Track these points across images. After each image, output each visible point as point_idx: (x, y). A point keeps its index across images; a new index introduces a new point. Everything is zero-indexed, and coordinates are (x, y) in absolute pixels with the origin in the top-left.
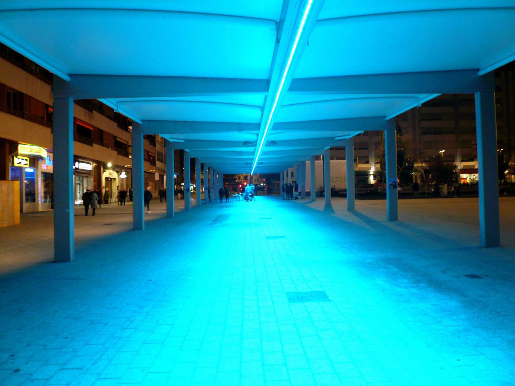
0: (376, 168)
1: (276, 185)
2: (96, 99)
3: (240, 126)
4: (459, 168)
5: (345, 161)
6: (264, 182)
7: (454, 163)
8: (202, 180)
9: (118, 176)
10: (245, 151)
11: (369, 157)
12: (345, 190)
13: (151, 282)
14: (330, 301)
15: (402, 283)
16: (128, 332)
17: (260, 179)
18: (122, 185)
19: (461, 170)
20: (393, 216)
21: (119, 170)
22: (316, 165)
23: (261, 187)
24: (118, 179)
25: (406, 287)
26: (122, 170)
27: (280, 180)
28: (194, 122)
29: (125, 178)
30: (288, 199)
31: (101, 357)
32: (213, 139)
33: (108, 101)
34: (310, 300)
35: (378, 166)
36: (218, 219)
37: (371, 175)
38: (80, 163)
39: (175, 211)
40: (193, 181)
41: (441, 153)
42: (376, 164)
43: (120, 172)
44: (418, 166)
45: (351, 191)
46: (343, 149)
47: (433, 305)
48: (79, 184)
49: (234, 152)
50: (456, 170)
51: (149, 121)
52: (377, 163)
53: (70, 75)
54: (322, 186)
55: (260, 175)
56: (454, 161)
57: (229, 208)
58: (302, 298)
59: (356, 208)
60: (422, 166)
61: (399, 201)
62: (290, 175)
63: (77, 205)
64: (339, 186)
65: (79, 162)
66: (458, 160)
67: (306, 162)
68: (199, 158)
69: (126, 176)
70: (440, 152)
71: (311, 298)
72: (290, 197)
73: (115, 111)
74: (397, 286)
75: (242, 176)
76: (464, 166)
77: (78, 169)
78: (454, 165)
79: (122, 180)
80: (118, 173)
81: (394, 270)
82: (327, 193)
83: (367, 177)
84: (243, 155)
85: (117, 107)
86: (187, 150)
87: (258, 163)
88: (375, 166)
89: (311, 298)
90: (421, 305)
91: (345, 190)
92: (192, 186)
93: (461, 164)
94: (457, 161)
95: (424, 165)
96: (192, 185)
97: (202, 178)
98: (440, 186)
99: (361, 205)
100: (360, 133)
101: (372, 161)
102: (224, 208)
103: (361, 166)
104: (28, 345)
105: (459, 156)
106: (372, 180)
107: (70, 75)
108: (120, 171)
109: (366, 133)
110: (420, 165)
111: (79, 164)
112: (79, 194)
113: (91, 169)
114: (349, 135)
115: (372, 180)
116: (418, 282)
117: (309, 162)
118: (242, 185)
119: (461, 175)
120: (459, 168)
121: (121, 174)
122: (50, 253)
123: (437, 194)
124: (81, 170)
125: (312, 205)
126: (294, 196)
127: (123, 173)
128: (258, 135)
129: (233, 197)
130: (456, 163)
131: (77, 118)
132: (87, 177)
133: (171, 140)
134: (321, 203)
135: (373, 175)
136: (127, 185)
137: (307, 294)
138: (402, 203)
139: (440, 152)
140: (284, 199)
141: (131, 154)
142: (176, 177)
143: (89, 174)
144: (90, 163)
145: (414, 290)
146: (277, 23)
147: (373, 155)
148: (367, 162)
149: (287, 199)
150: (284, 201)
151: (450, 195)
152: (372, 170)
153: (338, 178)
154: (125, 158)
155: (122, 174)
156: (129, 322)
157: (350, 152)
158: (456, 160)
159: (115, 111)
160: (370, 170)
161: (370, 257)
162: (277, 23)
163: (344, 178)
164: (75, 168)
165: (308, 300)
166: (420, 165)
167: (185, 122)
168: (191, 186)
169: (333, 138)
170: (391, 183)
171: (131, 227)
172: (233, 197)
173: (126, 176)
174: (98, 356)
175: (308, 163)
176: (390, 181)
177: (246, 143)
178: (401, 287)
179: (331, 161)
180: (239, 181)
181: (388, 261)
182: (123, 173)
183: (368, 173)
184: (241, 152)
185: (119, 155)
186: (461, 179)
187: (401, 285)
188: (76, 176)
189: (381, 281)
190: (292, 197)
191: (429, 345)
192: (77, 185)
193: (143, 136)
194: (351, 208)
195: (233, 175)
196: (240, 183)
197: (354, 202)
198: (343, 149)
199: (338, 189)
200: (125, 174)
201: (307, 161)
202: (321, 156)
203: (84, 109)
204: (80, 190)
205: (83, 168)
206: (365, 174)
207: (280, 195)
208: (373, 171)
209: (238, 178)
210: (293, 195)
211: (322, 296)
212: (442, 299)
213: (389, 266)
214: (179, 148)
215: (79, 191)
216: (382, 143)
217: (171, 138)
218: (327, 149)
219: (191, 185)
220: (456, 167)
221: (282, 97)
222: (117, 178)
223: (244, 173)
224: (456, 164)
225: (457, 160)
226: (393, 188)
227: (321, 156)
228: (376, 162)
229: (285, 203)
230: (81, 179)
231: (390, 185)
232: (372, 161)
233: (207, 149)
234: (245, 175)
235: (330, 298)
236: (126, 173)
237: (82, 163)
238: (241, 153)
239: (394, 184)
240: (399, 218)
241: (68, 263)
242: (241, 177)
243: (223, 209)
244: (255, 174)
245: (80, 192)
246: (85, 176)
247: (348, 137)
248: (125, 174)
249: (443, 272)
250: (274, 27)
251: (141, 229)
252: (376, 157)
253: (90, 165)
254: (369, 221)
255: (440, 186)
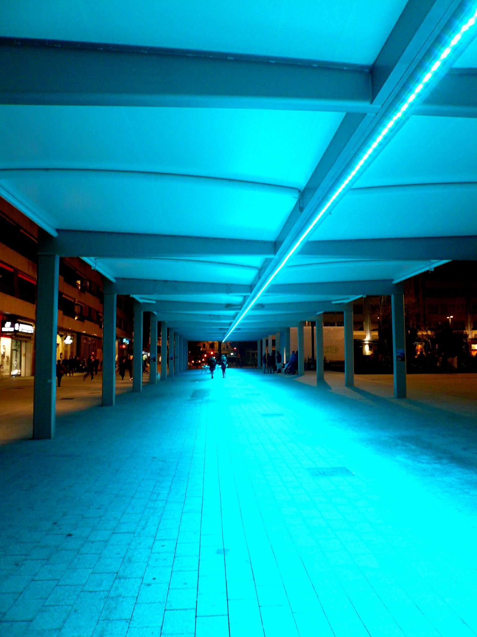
0: (372, 336)
1: (251, 355)
2: (79, 258)
3: (229, 288)
4: (470, 337)
5: (343, 327)
6: (234, 351)
7: (464, 331)
8: (159, 347)
9: (62, 341)
10: (222, 314)
11: (364, 323)
12: (343, 363)
13: (155, 459)
14: (354, 475)
15: (424, 459)
16: (161, 504)
17: (230, 347)
18: (66, 352)
19: (472, 339)
20: (402, 393)
21: (64, 334)
22: (305, 331)
23: (230, 357)
24: (62, 345)
25: (428, 463)
26: (68, 334)
27: (256, 349)
28: (176, 282)
29: (70, 343)
30: (269, 372)
31: (146, 523)
32: (191, 301)
33: (90, 259)
34: (334, 475)
35: (376, 333)
36: (196, 395)
37: (366, 344)
38: (21, 324)
39: (118, 385)
40: (147, 348)
41: (449, 319)
42: (372, 332)
43: (65, 336)
44: (423, 335)
45: (349, 365)
46: (342, 313)
47: (458, 479)
48: (16, 350)
49: (210, 315)
50: (466, 340)
51: (124, 279)
52: (374, 330)
53: (58, 230)
54: (310, 357)
55: (231, 342)
56: (465, 329)
57: (203, 382)
58: (324, 473)
59: (356, 383)
60: (428, 335)
61: (408, 376)
62: (270, 343)
63: (13, 375)
64: (332, 357)
65: (20, 323)
66: (469, 328)
67: (291, 328)
68: (166, 322)
69: (71, 341)
70: (448, 318)
71: (334, 473)
72: (272, 370)
73: (92, 269)
74: (419, 462)
75: (208, 343)
76: (476, 335)
77: (18, 331)
78: (464, 333)
79: (66, 345)
80: (62, 338)
81: (413, 447)
82: (319, 365)
83: (361, 347)
84: (221, 319)
85: (95, 264)
86: (155, 313)
87: (237, 329)
88: (371, 333)
89: (334, 473)
90: (446, 479)
91: (343, 363)
92: (146, 354)
93: (472, 334)
94: (468, 329)
95: (429, 333)
96: (146, 353)
97: (158, 345)
98: (449, 360)
99: (359, 379)
100: (362, 297)
101: (367, 327)
102: (197, 382)
103: (357, 334)
104: (64, 515)
105: (470, 322)
106: (367, 351)
107: (58, 230)
108: (64, 335)
109: (368, 296)
110: (425, 333)
111: (19, 326)
112: (15, 362)
113: (33, 332)
114: (348, 299)
115: (367, 351)
116: (439, 458)
117: (297, 328)
118: (207, 354)
119: (473, 345)
120: (470, 337)
121: (65, 339)
122: (28, 430)
123: (446, 369)
124: (22, 332)
125: (301, 379)
126: (278, 368)
127: (69, 337)
128: (245, 298)
129: (202, 368)
130: (467, 331)
131: (18, 270)
132: (26, 342)
133: (141, 301)
134: (311, 378)
135: (369, 344)
136: (72, 353)
137: (329, 470)
138: (410, 377)
139: (448, 318)
140: (265, 373)
141: (77, 315)
142: (128, 343)
143: (30, 338)
144: (31, 325)
145: (437, 466)
146: (299, 191)
147: (369, 320)
148: (362, 329)
149: (268, 373)
150: (265, 374)
151: (460, 370)
152: (368, 338)
153: (328, 347)
154: (71, 319)
155: (67, 338)
156: (155, 495)
157: (349, 317)
158: (466, 328)
159: (92, 269)
160: (365, 338)
161: (384, 435)
162: (299, 191)
163: (335, 348)
164: (15, 330)
165: (331, 475)
166: (425, 333)
167: (166, 281)
168: (145, 354)
169: (330, 301)
170: (399, 354)
171: (100, 402)
172: (202, 368)
173: (71, 341)
174: (143, 523)
175: (294, 330)
176: (397, 352)
177: (229, 306)
178: (422, 463)
179: (324, 327)
180: (205, 349)
181: (404, 439)
182: (69, 337)
183: (362, 342)
184: (218, 316)
185: (64, 316)
186: (473, 350)
187: (423, 461)
188: (13, 340)
189: (401, 458)
190: (275, 369)
191: (460, 511)
192: (13, 351)
193: (116, 296)
194: (350, 384)
195: (198, 342)
196: (205, 352)
197: (353, 377)
198: (342, 313)
199: (330, 361)
200: (71, 339)
201: (291, 327)
202: (307, 322)
203: (27, 260)
204: (16, 358)
205: (23, 331)
206: (359, 344)
207: (257, 367)
208: (368, 340)
209: (202, 346)
210: (276, 367)
211: (345, 471)
212: (467, 473)
213: (407, 444)
214: (148, 309)
215: (15, 359)
216: (381, 306)
217: (141, 298)
218: (320, 315)
219: (143, 353)
220: (467, 336)
221: (291, 259)
222: (61, 343)
223: (215, 340)
224: (466, 333)
225: (468, 327)
226: (325, 360)
227: (307, 322)
228: (372, 329)
229: (267, 377)
230: (19, 343)
231: (397, 357)
232: (367, 327)
233: (179, 312)
234: (211, 342)
235: (354, 473)
236: (72, 337)
237: (23, 324)
238: (218, 317)
239: (402, 356)
240: (407, 397)
241: (48, 440)
242: (207, 345)
243: (195, 383)
244: (226, 342)
245: (16, 360)
246: (24, 341)
247: (346, 301)
248: (71, 339)
249: (465, 449)
250: (297, 195)
251: (111, 404)
252: (373, 322)
253: (31, 326)
254: (375, 398)
255: (449, 360)
